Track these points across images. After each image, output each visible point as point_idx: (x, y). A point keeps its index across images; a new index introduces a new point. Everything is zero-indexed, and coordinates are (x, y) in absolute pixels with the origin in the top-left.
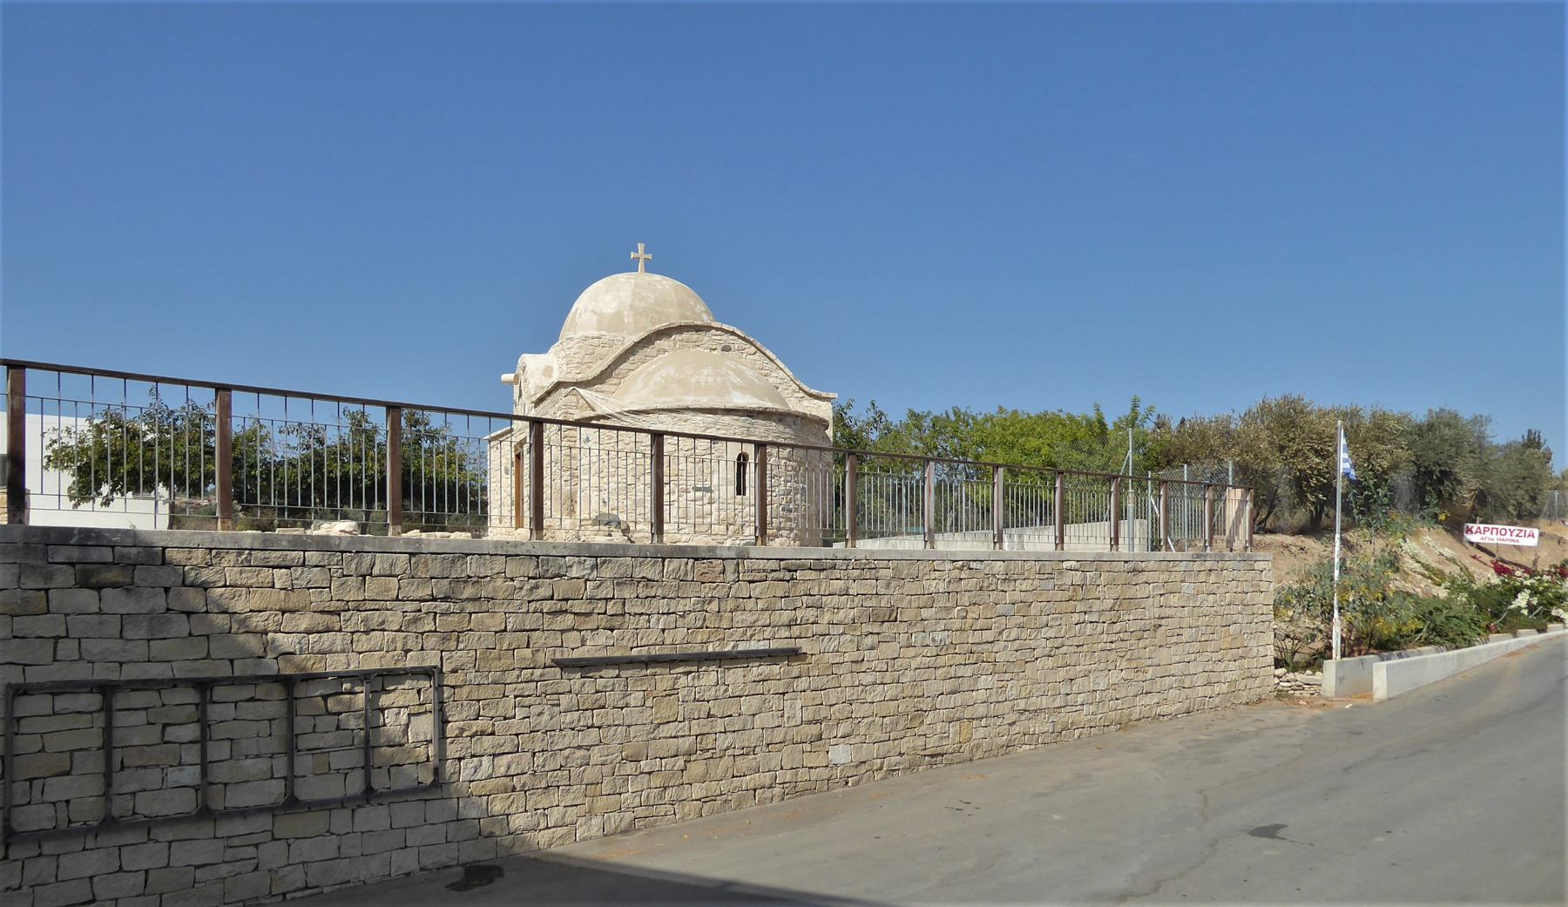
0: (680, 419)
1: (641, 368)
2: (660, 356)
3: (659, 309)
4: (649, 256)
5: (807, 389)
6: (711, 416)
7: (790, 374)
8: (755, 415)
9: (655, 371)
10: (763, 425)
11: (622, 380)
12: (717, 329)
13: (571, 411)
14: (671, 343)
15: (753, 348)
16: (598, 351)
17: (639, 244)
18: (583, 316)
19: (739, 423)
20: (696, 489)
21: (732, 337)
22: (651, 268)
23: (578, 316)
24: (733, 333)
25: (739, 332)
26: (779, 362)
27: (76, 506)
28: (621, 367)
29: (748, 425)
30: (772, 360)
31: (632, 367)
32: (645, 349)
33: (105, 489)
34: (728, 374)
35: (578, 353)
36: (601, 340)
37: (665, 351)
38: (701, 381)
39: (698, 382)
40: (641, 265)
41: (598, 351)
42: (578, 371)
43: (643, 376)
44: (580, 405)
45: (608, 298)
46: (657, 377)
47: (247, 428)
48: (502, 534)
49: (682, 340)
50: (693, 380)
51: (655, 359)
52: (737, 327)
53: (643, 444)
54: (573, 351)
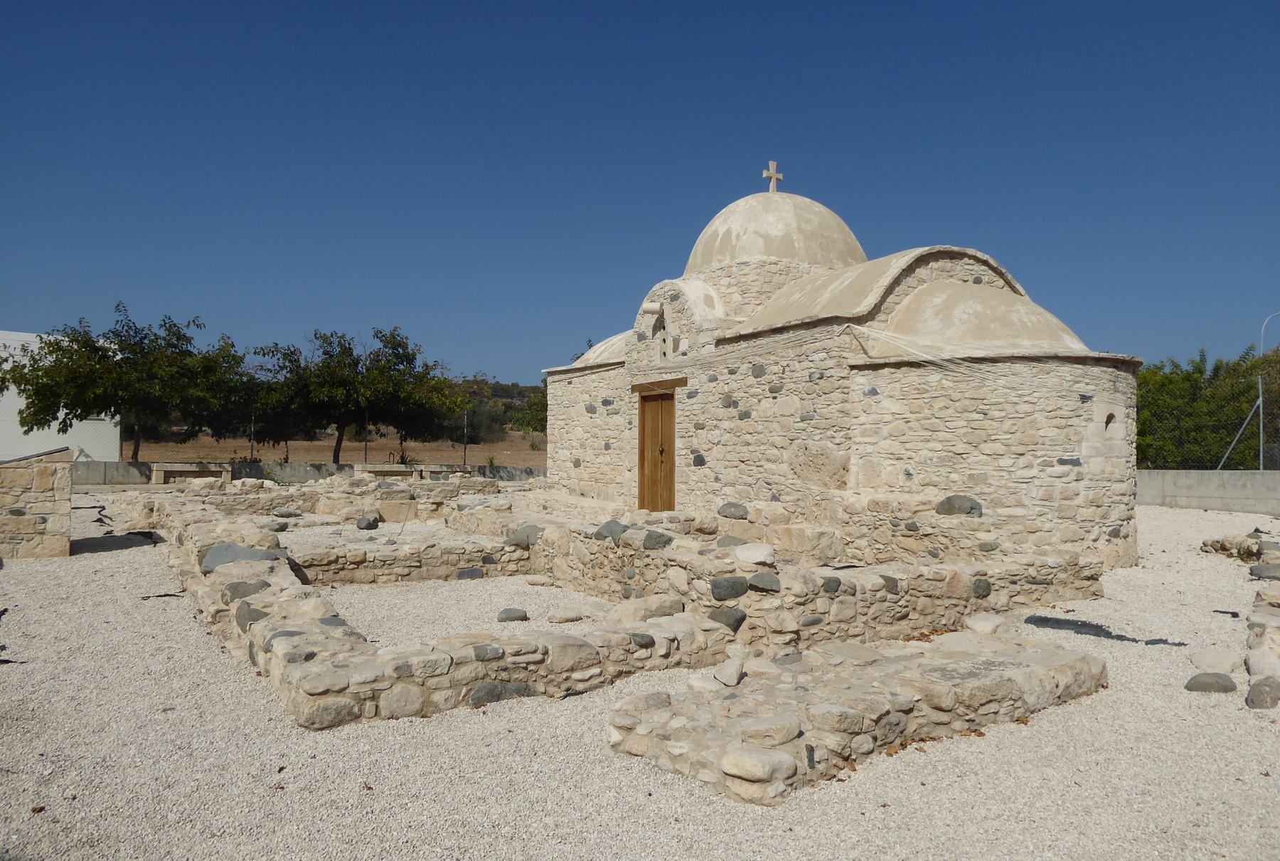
0: (1041, 370)
3: (825, 234)
4: (780, 176)
6: (1081, 366)
11: (890, 316)
13: (845, 354)
14: (929, 272)
16: (777, 278)
20: (1062, 462)
22: (782, 187)
24: (985, 263)
25: (992, 262)
27: (26, 433)
29: (1113, 379)
33: (61, 414)
35: (757, 280)
40: (772, 184)
41: (777, 278)
42: (757, 302)
47: (735, 395)
48: (581, 480)
53: (985, 401)
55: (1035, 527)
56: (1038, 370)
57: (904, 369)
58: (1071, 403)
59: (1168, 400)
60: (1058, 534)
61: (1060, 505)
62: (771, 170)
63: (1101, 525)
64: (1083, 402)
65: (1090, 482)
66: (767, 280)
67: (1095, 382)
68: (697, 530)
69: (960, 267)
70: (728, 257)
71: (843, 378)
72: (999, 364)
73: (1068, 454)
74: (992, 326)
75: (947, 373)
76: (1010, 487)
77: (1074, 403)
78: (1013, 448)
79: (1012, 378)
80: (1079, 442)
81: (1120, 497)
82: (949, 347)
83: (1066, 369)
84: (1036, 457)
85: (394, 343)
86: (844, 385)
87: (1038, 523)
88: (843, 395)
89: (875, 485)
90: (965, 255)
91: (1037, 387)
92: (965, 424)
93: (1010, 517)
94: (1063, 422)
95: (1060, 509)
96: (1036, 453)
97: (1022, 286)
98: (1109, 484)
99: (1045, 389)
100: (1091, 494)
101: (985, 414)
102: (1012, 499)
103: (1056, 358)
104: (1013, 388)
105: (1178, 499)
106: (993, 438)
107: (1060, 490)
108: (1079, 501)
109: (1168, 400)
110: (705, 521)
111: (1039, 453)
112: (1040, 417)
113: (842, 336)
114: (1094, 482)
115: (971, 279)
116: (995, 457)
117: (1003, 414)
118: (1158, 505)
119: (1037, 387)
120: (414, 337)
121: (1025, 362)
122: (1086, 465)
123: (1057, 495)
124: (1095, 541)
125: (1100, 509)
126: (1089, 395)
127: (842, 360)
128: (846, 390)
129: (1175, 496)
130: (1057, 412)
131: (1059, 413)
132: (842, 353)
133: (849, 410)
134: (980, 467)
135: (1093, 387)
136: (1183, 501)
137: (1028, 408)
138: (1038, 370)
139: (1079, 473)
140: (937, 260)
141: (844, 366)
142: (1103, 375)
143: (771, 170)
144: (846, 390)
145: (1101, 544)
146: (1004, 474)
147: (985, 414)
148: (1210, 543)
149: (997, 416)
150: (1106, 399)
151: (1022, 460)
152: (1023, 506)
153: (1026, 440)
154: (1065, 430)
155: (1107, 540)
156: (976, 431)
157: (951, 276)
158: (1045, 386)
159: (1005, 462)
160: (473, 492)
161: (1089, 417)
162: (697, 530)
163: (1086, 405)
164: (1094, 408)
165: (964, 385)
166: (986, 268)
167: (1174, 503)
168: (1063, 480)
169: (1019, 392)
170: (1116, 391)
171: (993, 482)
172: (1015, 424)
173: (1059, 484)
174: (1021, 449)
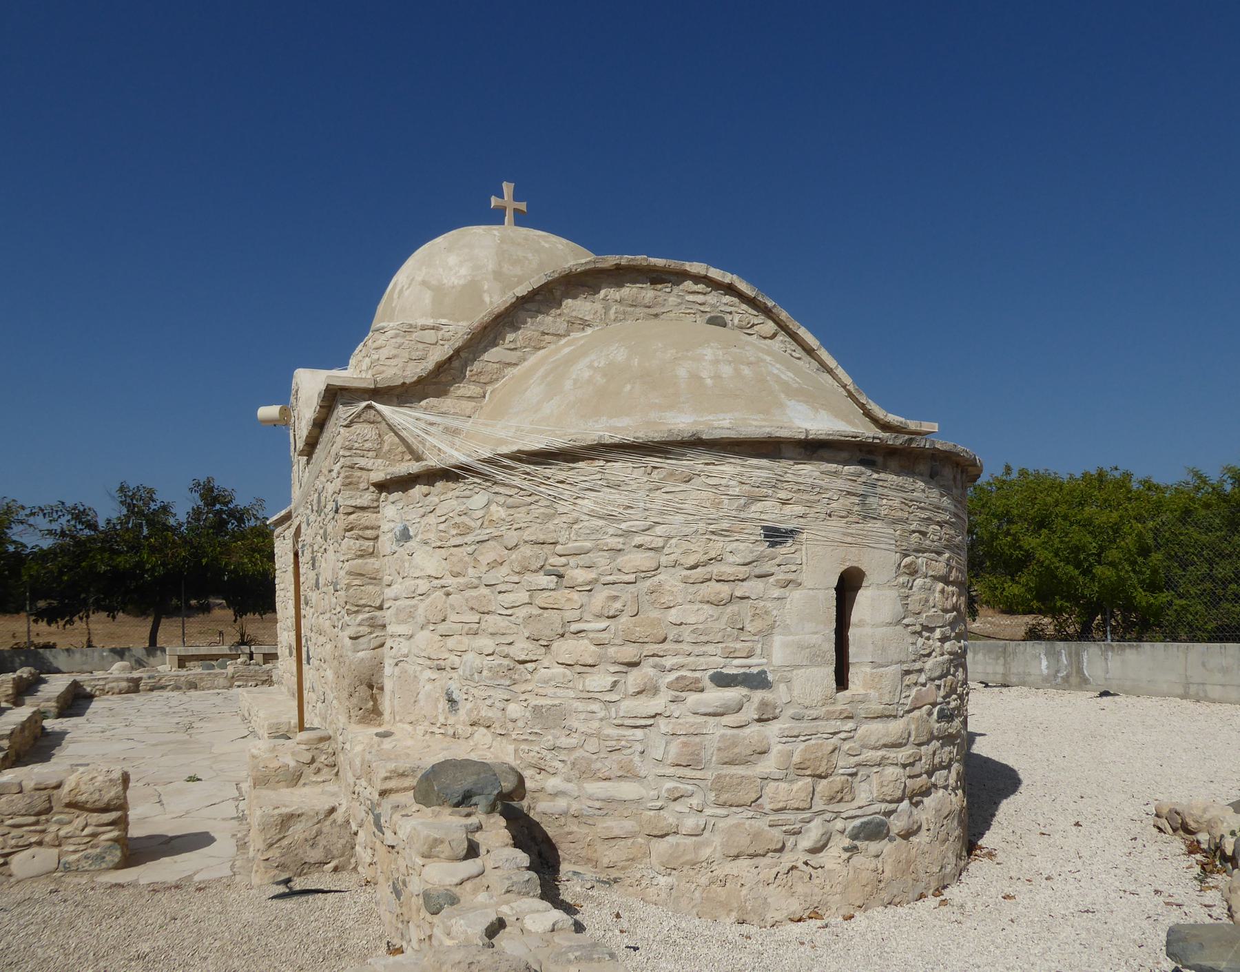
0: (672, 474)
1: (533, 359)
2: (573, 335)
4: (523, 206)
5: (879, 412)
6: (764, 462)
7: (847, 380)
8: (880, 460)
9: (570, 361)
10: (901, 489)
11: (489, 389)
12: (697, 279)
13: (362, 462)
14: (598, 306)
15: (771, 324)
17: (505, 184)
18: (407, 293)
19: (840, 483)
20: (722, 680)
21: (727, 299)
22: (521, 220)
23: (395, 296)
24: (730, 289)
25: (743, 286)
26: (824, 355)
28: (486, 356)
29: (861, 489)
30: (810, 352)
31: (512, 357)
32: (540, 317)
34: (763, 360)
35: (394, 357)
36: (440, 333)
37: (585, 324)
38: (704, 374)
39: (695, 377)
43: (542, 371)
44: (386, 447)
45: (452, 260)
46: (581, 370)
49: (620, 302)
50: (682, 372)
51: (563, 341)
52: (739, 275)
53: (559, 549)
54: (384, 353)
56: (663, 473)
57: (418, 490)
58: (742, 546)
59: (1195, 535)
60: (717, 840)
61: (719, 777)
62: (506, 197)
63: (828, 816)
64: (773, 545)
65: (794, 724)
67: (806, 497)
68: (70, 805)
69: (671, 296)
71: (363, 509)
72: (581, 464)
73: (736, 662)
74: (628, 387)
75: (497, 489)
76: (608, 738)
77: (747, 546)
78: (612, 651)
79: (613, 495)
80: (766, 634)
81: (880, 753)
83: (729, 469)
84: (663, 669)
85: (210, 495)
87: (669, 818)
88: (361, 542)
89: (413, 719)
90: (683, 276)
91: (662, 513)
92: (523, 597)
93: (609, 800)
94: (725, 589)
95: (719, 785)
96: (663, 661)
98: (850, 725)
99: (679, 518)
100: (799, 751)
101: (560, 576)
102: (610, 765)
104: (609, 517)
105: (1208, 688)
106: (575, 627)
107: (716, 745)
108: (768, 765)
109: (1195, 535)
110: (83, 788)
111: (669, 662)
112: (670, 580)
113: (355, 426)
114: (804, 724)
116: (578, 669)
117: (591, 575)
118: (1178, 696)
119: (662, 513)
120: (221, 483)
121: (635, 457)
122: (782, 687)
123: (711, 753)
124: (815, 851)
125: (824, 782)
126: (790, 526)
127: (359, 473)
128: (369, 533)
129: (1203, 684)
130: (709, 568)
131: (715, 569)
132: (357, 460)
133: (378, 571)
134: (550, 691)
135: (799, 509)
136: (1215, 692)
137: (642, 560)
138: (663, 473)
139: (764, 705)
140: (620, 285)
141: (362, 486)
142: (825, 482)
143: (506, 197)
144: (369, 533)
145: (832, 857)
146: (595, 707)
147: (560, 576)
148: (1165, 811)
149: (580, 580)
150: (837, 537)
151: (634, 679)
152: (636, 777)
153: (639, 632)
154: (730, 609)
155: (846, 850)
156: (546, 614)
157: (656, 315)
158: (678, 511)
159: (599, 681)
160: (254, 683)
161: (791, 576)
162: (70, 805)
163: (781, 550)
164: (802, 556)
165: (520, 515)
166: (736, 300)
167: (1202, 694)
168: (726, 720)
169: (624, 526)
170: (868, 516)
171: (576, 724)
172: (615, 598)
173: (716, 730)
174: (630, 653)
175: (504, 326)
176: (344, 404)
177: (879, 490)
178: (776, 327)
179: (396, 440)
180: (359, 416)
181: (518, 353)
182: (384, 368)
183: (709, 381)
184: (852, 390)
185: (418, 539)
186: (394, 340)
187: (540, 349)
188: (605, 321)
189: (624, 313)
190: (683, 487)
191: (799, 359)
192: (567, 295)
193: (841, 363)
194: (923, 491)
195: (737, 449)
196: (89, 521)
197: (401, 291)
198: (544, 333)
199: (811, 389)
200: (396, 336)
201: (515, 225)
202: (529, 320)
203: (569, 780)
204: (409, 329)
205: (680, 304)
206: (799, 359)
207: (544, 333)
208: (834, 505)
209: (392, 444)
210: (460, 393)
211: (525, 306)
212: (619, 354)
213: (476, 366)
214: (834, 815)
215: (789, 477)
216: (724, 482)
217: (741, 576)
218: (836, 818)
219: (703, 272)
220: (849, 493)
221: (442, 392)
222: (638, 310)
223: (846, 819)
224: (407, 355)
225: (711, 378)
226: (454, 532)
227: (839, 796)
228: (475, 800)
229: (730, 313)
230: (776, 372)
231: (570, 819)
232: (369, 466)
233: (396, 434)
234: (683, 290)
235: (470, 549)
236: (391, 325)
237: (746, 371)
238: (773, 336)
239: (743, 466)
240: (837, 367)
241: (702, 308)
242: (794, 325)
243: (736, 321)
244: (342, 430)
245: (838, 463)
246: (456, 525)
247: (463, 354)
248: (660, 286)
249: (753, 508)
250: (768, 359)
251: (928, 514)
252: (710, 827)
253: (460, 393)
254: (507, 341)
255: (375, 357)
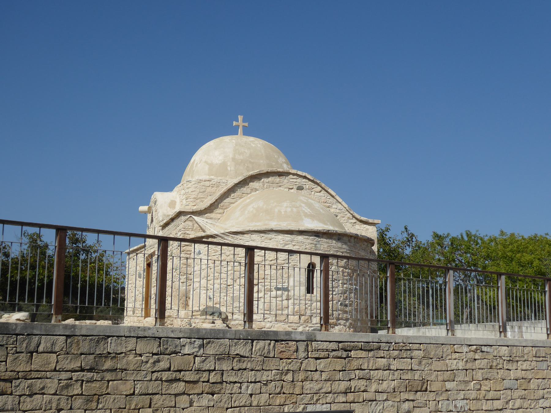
0: (267, 238)
2: (253, 193)
3: (252, 161)
4: (246, 124)
5: (358, 217)
6: (289, 236)
7: (346, 206)
8: (321, 235)
11: (226, 210)
12: (294, 174)
13: (188, 232)
14: (261, 184)
16: (209, 190)
17: (239, 116)
18: (199, 165)
19: (309, 241)
22: (247, 132)
23: (194, 166)
24: (305, 177)
25: (309, 177)
26: (338, 198)
28: (225, 201)
29: (315, 243)
30: (333, 196)
31: (233, 201)
35: (194, 191)
37: (256, 190)
38: (282, 211)
39: (280, 212)
40: (240, 130)
41: (209, 190)
42: (193, 204)
44: (195, 228)
46: (250, 208)
50: (276, 210)
54: (190, 190)
55: (261, 325)
56: (265, 238)
62: (240, 122)
63: (304, 326)
66: (202, 191)
67: (299, 244)
70: (190, 177)
72: (245, 235)
74: (261, 214)
82: (289, 227)
86: (187, 249)
88: (186, 255)
97: (332, 190)
103: (272, 231)
113: (186, 222)
115: (295, 187)
121: (258, 234)
127: (187, 235)
128: (189, 252)
132: (186, 231)
138: (265, 238)
140: (268, 177)
143: (240, 122)
144: (189, 252)
157: (280, 186)
161: (296, 264)
166: (307, 180)
175: (231, 192)
176: (184, 216)
177: (320, 243)
178: (321, 189)
179: (198, 226)
180: (188, 219)
181: (235, 200)
182: (190, 195)
183: (283, 213)
184: (348, 209)
185: (203, 254)
186: (194, 185)
187: (242, 198)
188: (263, 188)
189: (269, 186)
190: (269, 241)
191: (329, 199)
192: (251, 181)
193: (343, 200)
194: (335, 243)
195: (282, 232)
196: (6, 252)
197: (197, 164)
198: (243, 193)
199: (314, 214)
200: (195, 184)
201: (243, 135)
202: (238, 190)
203: (239, 315)
204: (200, 181)
205: (288, 182)
206: (329, 199)
207: (243, 193)
208: (307, 246)
209: (196, 227)
210: (217, 212)
211: (238, 186)
212: (261, 204)
213: (222, 204)
214: (306, 326)
215: (295, 239)
216: (279, 240)
217: (282, 263)
218: (306, 327)
219: (296, 173)
220: (311, 243)
221: (211, 212)
222: (274, 185)
223: (309, 327)
224: (198, 191)
225: (284, 212)
226: (213, 252)
227: (307, 321)
228: (215, 314)
229: (305, 185)
230: (304, 209)
231: (239, 326)
232: (190, 233)
233: (198, 224)
234: (289, 178)
235: (217, 256)
236: (193, 180)
237: (295, 210)
238: (320, 192)
239: (284, 236)
240: (342, 202)
241: (295, 183)
242: (327, 188)
243: (307, 187)
244: (183, 223)
245: (308, 236)
246: (214, 250)
247: (218, 201)
248: (281, 177)
249: (286, 247)
250: (303, 205)
251: (337, 249)
252: (273, 326)
253: (217, 212)
254: (231, 196)
255: (187, 191)
